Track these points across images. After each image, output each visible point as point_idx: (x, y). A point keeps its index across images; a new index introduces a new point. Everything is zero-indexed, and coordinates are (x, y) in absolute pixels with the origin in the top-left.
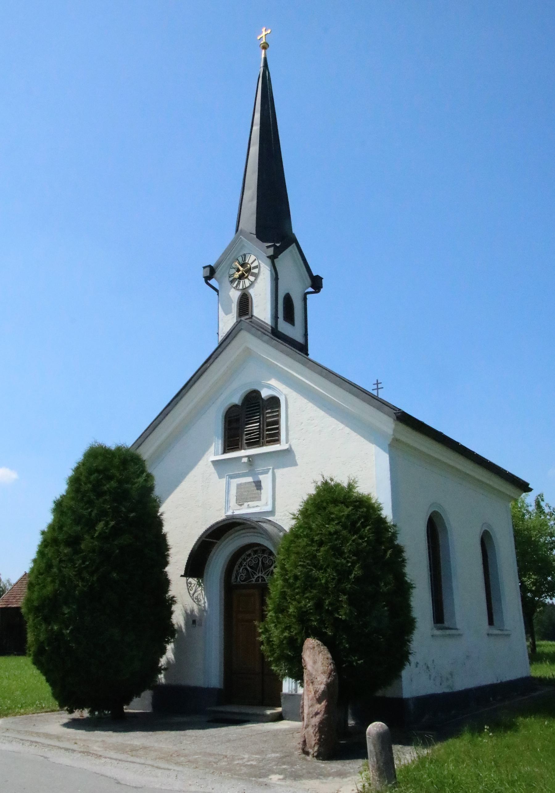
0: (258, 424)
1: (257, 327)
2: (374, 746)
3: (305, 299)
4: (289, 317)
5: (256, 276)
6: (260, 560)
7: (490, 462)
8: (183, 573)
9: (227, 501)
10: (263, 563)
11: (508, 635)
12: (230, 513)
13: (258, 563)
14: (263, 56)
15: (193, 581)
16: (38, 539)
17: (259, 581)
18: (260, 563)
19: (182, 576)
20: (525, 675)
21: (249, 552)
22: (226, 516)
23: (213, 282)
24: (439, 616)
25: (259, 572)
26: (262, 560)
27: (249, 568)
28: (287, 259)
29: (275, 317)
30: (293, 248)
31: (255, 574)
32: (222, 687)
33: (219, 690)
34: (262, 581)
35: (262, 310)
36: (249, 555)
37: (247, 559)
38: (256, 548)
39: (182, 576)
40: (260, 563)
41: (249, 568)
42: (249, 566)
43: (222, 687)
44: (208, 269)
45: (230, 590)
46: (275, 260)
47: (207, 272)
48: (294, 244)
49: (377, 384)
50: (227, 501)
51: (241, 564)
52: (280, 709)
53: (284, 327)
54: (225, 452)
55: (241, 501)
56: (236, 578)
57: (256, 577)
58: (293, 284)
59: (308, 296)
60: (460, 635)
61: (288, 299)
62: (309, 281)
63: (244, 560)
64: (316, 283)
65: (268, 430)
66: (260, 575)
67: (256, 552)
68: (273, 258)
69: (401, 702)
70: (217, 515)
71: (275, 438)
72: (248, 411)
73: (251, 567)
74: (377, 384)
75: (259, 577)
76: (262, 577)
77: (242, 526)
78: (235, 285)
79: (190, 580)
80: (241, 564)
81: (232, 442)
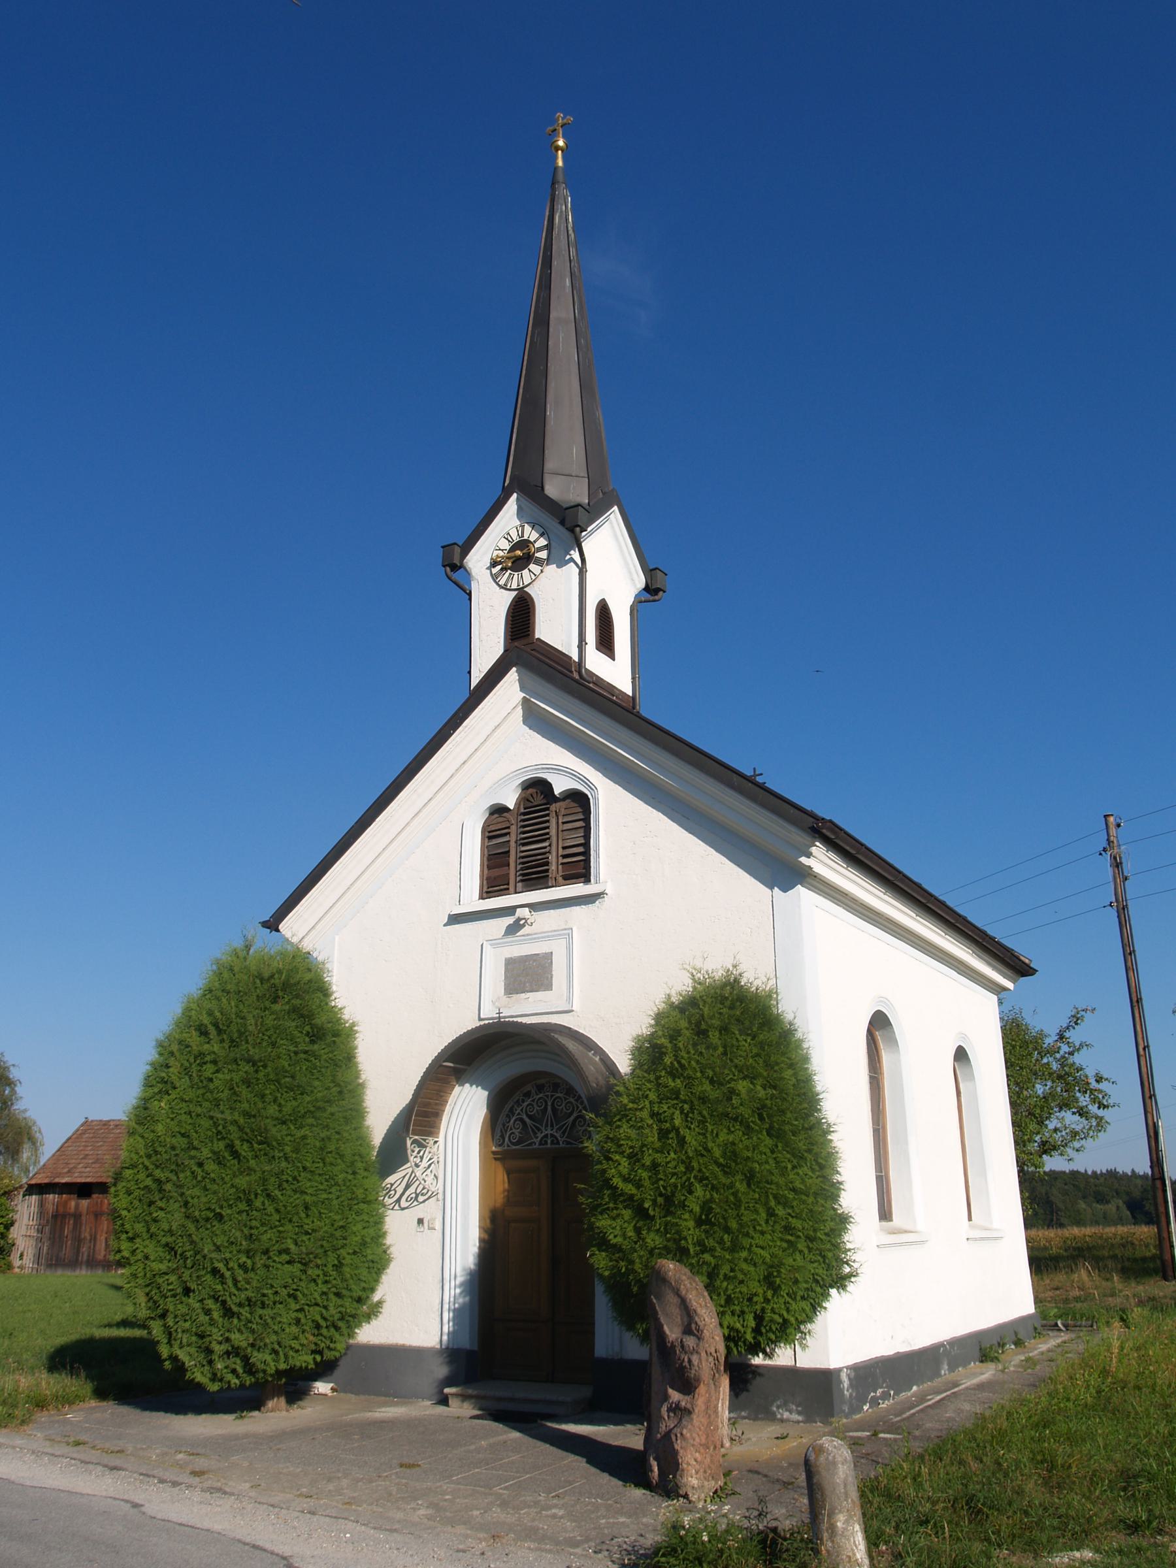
0: (581, 858)
6: (524, 1117)
7: (185, 1413)
10: (554, 1110)
12: (489, 1012)
13: (546, 1108)
16: (178, 1010)
17: (546, 1143)
18: (549, 1108)
21: (528, 1088)
24: (885, 1214)
25: (547, 1126)
26: (553, 1104)
27: (527, 1120)
31: (539, 1129)
32: (476, 1348)
34: (552, 1143)
37: (523, 1101)
38: (542, 1081)
40: (549, 1108)
41: (527, 1120)
42: (528, 1115)
43: (476, 1348)
52: (1009, 985)
57: (540, 1136)
66: (549, 1132)
67: (540, 1088)
69: (824, 1379)
72: (505, 834)
75: (546, 1136)
76: (552, 1135)
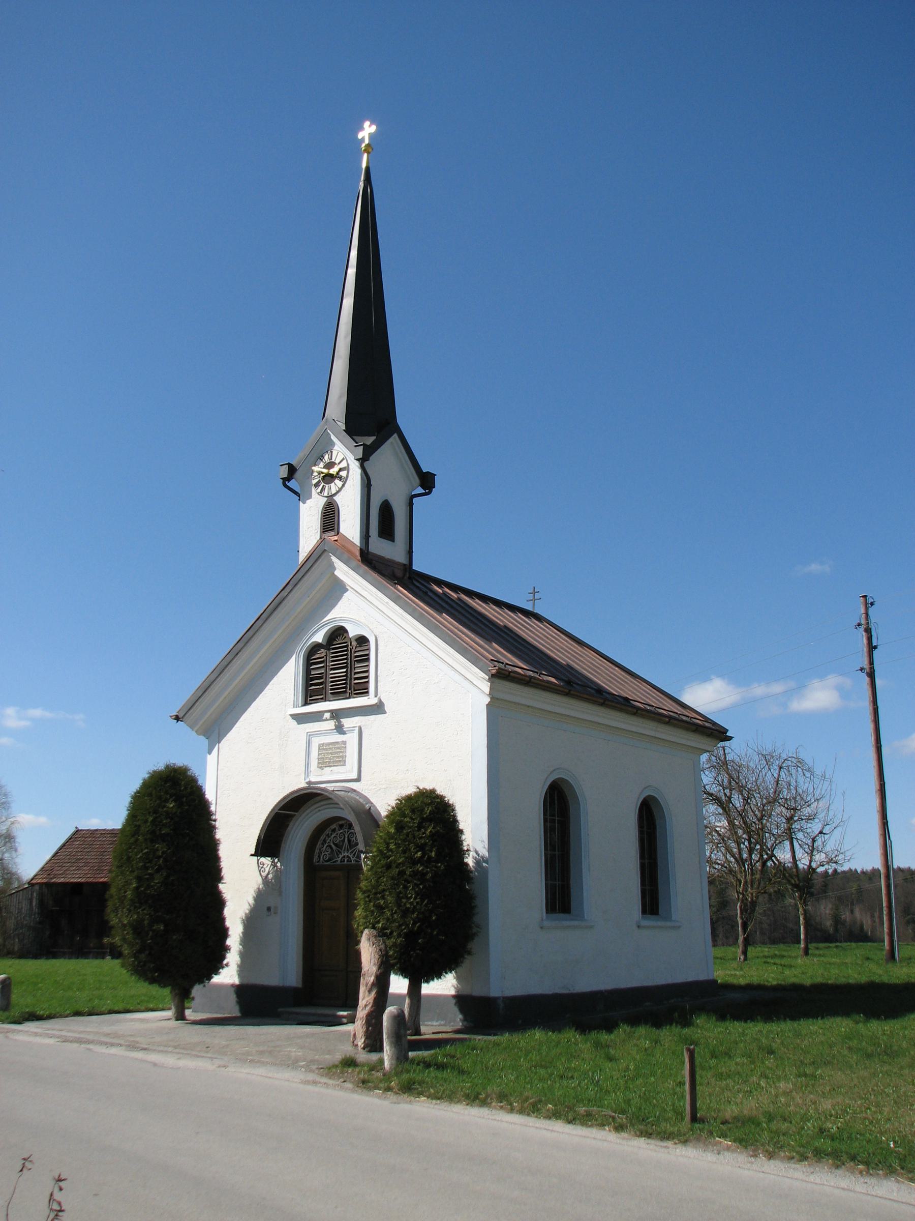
1: (343, 550)
2: (391, 1047)
3: (411, 504)
4: (387, 530)
5: (345, 480)
8: (253, 853)
9: (307, 765)
11: (679, 927)
14: (364, 165)
15: (267, 861)
19: (252, 855)
20: (702, 977)
21: (333, 827)
22: (309, 783)
23: (292, 484)
28: (389, 451)
29: (365, 535)
30: (395, 438)
32: (300, 986)
33: (295, 990)
35: (350, 526)
36: (334, 830)
38: (341, 823)
39: (252, 855)
43: (300, 986)
44: (286, 468)
45: (313, 872)
46: (366, 464)
47: (284, 472)
48: (395, 435)
49: (534, 593)
50: (307, 765)
51: (325, 841)
53: (379, 547)
54: (306, 703)
55: (322, 764)
56: (319, 857)
57: (341, 856)
58: (394, 484)
59: (415, 500)
60: (591, 927)
61: (386, 511)
62: (417, 480)
63: (328, 836)
64: (427, 481)
65: (355, 679)
66: (346, 854)
68: (363, 461)
70: (296, 783)
71: (362, 690)
73: (336, 845)
74: (534, 593)
77: (319, 798)
78: (319, 490)
79: (263, 860)
80: (325, 841)
81: (313, 688)
